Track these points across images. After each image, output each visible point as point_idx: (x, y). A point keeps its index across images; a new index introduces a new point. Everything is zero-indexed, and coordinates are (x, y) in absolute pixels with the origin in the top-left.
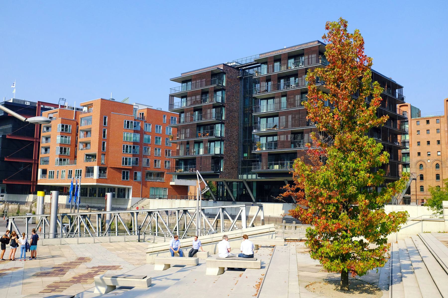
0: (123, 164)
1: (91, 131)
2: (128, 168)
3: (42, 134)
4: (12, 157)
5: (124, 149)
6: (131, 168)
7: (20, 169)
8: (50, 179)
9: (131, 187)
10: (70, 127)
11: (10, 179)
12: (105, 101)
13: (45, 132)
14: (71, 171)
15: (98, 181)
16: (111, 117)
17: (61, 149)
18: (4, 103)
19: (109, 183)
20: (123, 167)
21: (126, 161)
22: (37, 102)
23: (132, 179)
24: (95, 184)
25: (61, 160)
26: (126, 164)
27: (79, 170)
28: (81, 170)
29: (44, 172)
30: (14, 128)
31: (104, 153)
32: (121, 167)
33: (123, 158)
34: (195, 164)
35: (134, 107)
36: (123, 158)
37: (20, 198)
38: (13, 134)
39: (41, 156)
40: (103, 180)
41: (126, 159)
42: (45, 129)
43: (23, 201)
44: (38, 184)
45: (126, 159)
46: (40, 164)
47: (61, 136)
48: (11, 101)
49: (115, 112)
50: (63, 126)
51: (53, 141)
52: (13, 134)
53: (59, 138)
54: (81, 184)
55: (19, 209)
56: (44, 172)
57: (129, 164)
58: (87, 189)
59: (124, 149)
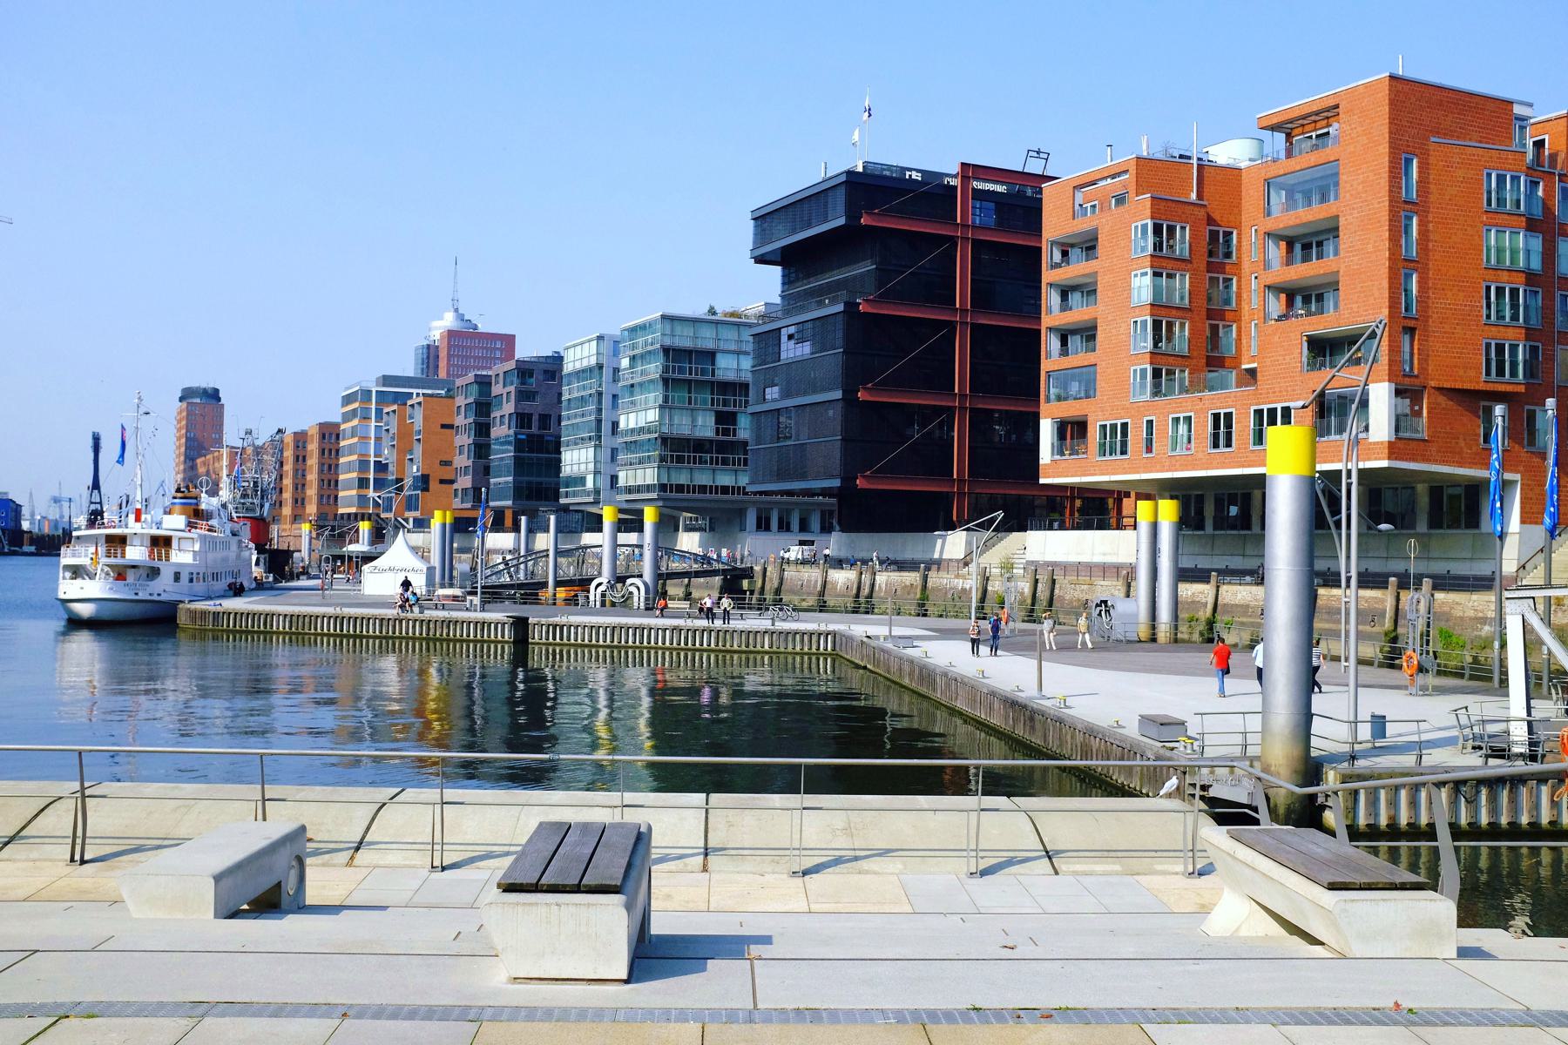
0: (1488, 373)
1: (1337, 229)
2: (1509, 388)
3: (1048, 276)
4: (884, 386)
5: (1489, 307)
6: (1522, 389)
7: (909, 432)
8: (1108, 457)
9: (1518, 477)
10: (1183, 236)
11: (879, 471)
12: (1406, 88)
13: (1058, 266)
14: (1229, 416)
15: (1393, 450)
16: (1432, 160)
17: (1157, 325)
18: (843, 178)
19: (1436, 462)
20: (1490, 387)
21: (1498, 359)
22: (955, 169)
23: (1521, 444)
24: (1384, 464)
25: (1157, 374)
26: (1501, 372)
27: (1114, 427)
28: (1125, 426)
29: (1072, 431)
30: (882, 275)
31: (1411, 324)
32: (1482, 387)
33: (1488, 346)
34: (1344, 401)
35: (1517, 110)
36: (1488, 346)
37: (909, 545)
38: (885, 297)
39: (1046, 365)
40: (1413, 445)
41: (1500, 349)
42: (1057, 257)
43: (918, 556)
44: (1042, 481)
45: (1500, 349)
46: (1048, 400)
47: (1157, 274)
48: (860, 169)
49: (1445, 135)
50: (1157, 230)
51: (1116, 294)
52: (880, 296)
53: (1142, 286)
54: (1361, 465)
55: (924, 587)
56: (1072, 431)
57: (1514, 373)
58: (1200, 499)
59: (1489, 307)
